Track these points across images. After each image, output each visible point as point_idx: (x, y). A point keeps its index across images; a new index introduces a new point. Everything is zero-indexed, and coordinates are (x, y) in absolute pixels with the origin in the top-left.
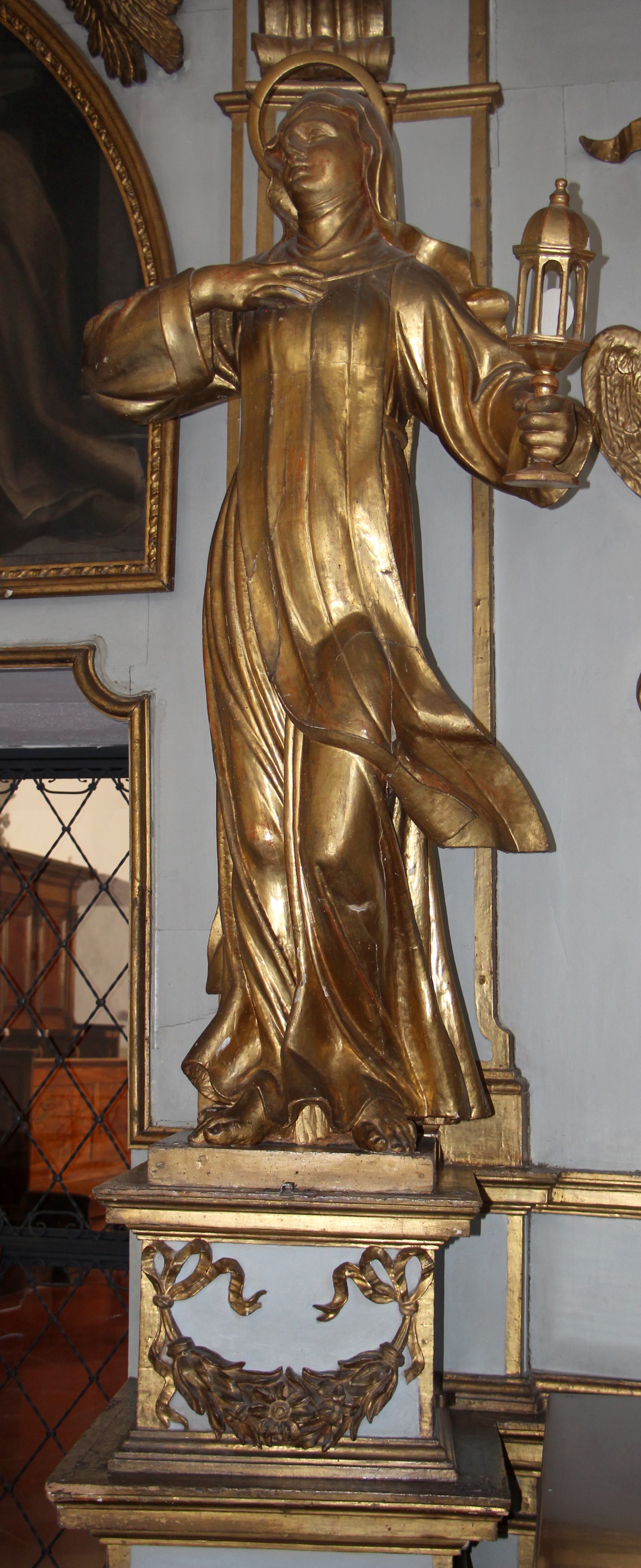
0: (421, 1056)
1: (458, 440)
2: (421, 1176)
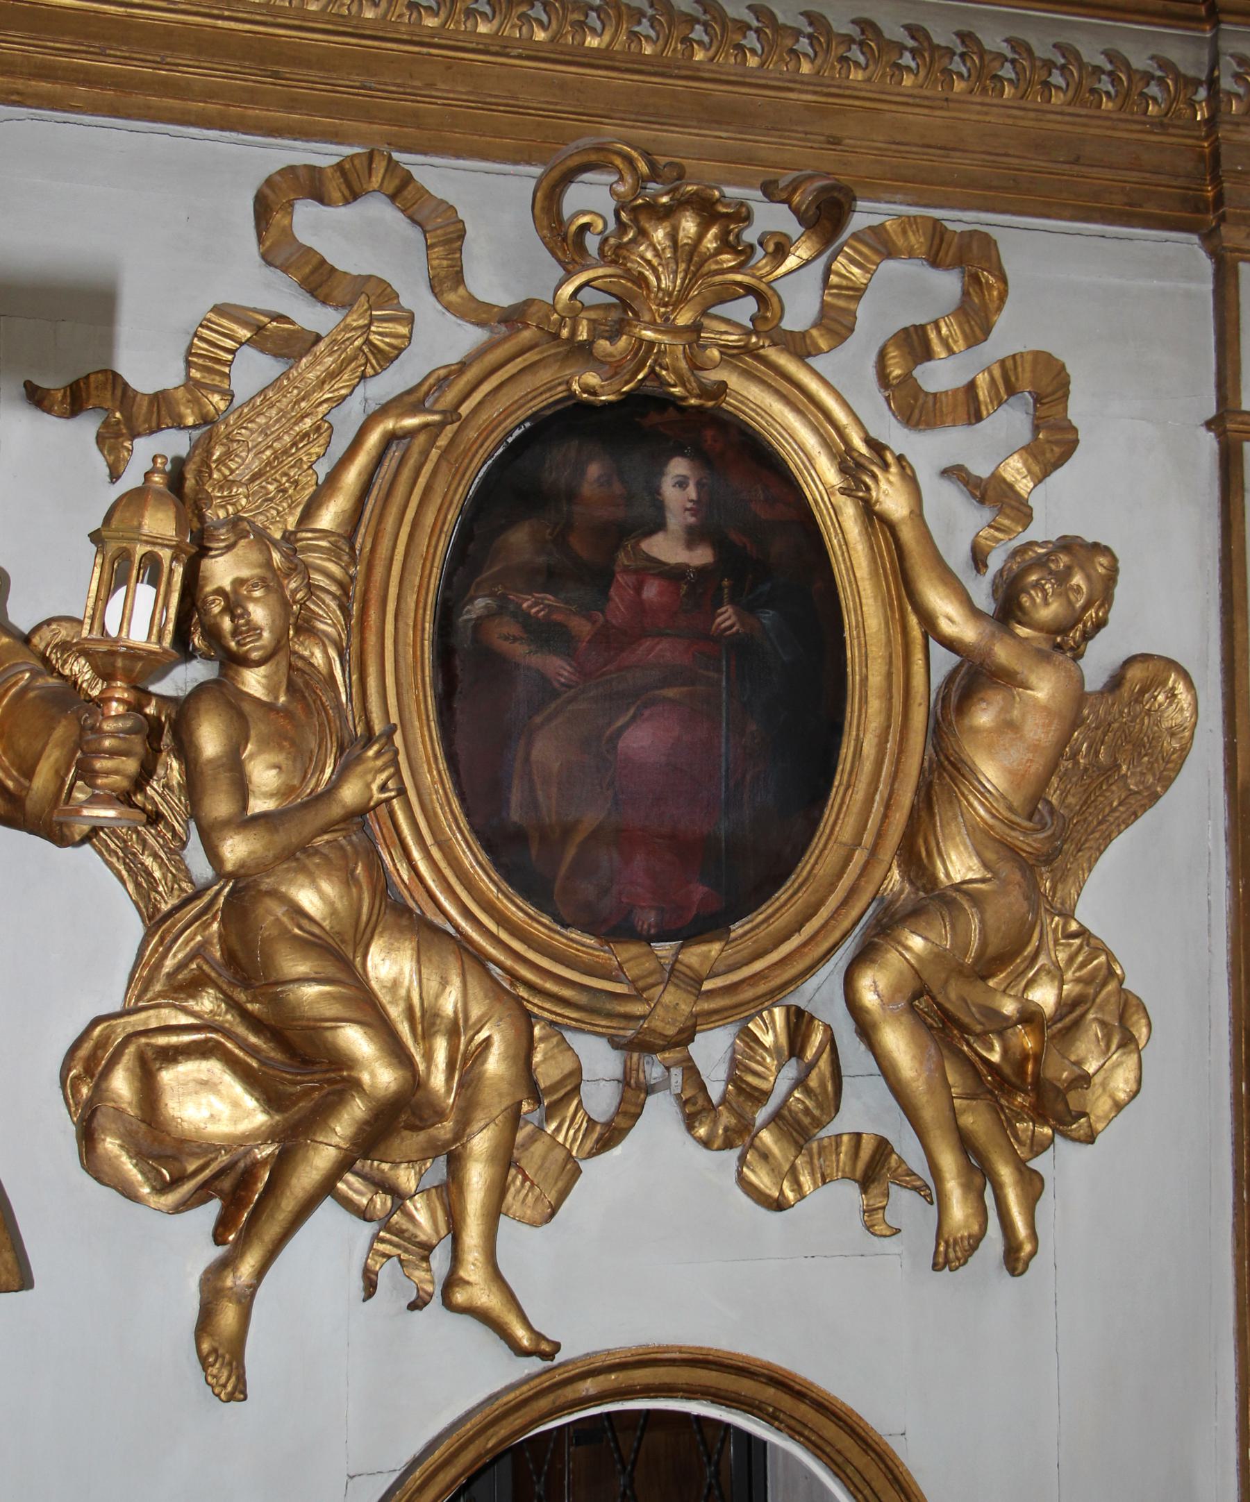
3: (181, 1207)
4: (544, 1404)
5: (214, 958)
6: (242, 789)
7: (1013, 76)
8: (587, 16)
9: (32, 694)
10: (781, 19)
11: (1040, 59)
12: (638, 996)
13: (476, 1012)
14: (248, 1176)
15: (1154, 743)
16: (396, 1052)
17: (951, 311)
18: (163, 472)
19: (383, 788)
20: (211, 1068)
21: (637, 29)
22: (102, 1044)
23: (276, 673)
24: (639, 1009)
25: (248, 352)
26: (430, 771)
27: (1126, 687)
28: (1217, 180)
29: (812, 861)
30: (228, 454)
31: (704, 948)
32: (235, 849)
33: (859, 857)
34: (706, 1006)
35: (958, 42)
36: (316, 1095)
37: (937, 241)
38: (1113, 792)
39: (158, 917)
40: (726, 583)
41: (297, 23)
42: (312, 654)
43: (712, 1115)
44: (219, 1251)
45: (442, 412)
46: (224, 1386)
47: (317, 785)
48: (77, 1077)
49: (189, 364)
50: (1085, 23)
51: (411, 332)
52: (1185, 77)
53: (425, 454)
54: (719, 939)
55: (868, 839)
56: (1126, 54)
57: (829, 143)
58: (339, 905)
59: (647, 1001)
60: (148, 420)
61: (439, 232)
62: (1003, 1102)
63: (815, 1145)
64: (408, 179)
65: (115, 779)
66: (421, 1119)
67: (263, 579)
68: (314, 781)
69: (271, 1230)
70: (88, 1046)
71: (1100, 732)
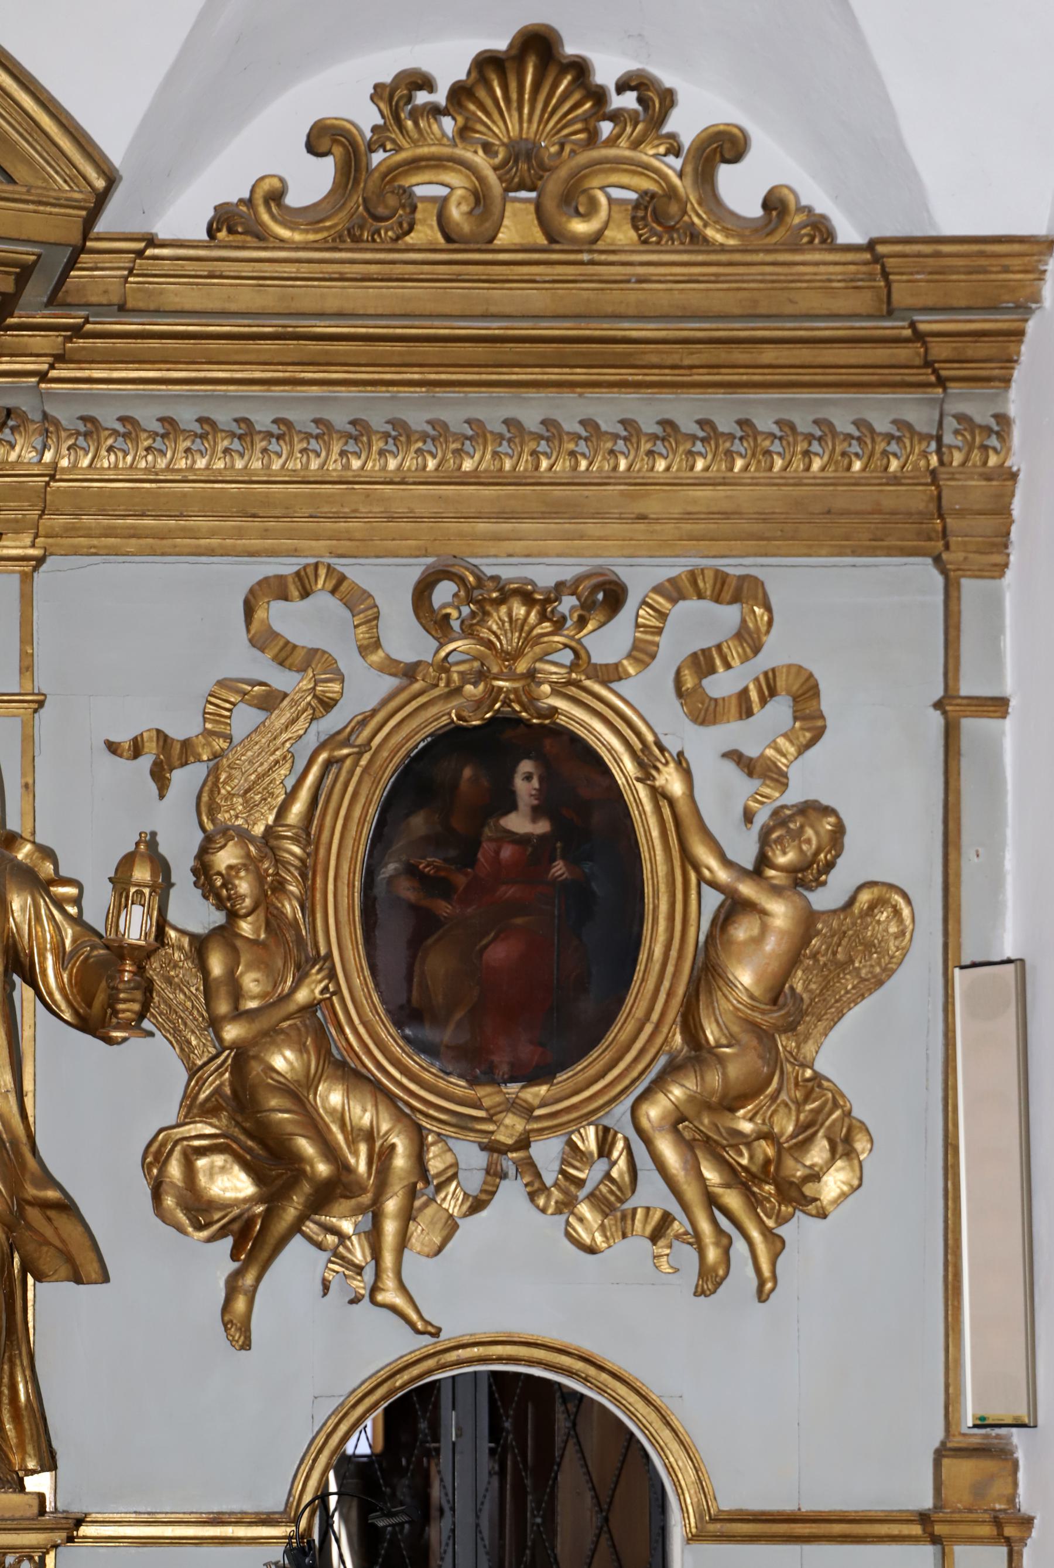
0: (15, 1428)
1: (50, 994)
2: (31, 1506)
3: (210, 1240)
4: (431, 1363)
5: (226, 1095)
6: (237, 993)
7: (781, 450)
8: (463, 444)
9: (91, 960)
10: (604, 427)
11: (802, 433)
12: (490, 1119)
13: (385, 1127)
14: (250, 1223)
15: (883, 944)
16: (330, 1152)
17: (730, 635)
18: (145, 842)
19: (322, 992)
20: (219, 1160)
21: (499, 449)
22: (163, 1144)
23: (257, 920)
24: (491, 1127)
25: (241, 706)
26: (359, 977)
27: (857, 904)
28: (941, 516)
29: (616, 1030)
30: (230, 777)
31: (535, 1089)
32: (231, 1032)
33: (648, 1029)
34: (536, 1126)
35: (738, 428)
36: (285, 1177)
37: (718, 586)
38: (847, 980)
39: (195, 1069)
40: (559, 844)
41: (265, 479)
42: (283, 906)
43: (546, 1193)
44: (236, 1265)
45: (359, 746)
46: (237, 1341)
47: (283, 990)
48: (150, 1163)
49: (205, 720)
50: (841, 399)
51: (342, 688)
52: (920, 434)
53: (351, 773)
54: (545, 1083)
55: (655, 1016)
56: (871, 421)
57: (146, 934)
58: (296, 1064)
59: (495, 1122)
60: (180, 758)
61: (362, 616)
62: (755, 1189)
63: (619, 1214)
64: (342, 578)
65: (128, 1014)
66: (351, 1192)
67: (244, 865)
68: (280, 989)
69: (264, 1255)
70: (156, 1145)
71: (835, 939)
